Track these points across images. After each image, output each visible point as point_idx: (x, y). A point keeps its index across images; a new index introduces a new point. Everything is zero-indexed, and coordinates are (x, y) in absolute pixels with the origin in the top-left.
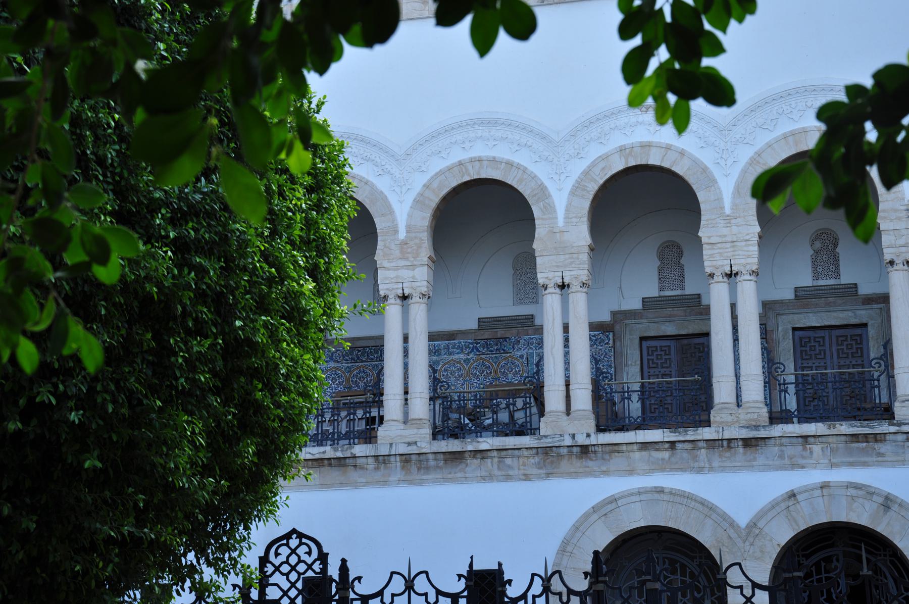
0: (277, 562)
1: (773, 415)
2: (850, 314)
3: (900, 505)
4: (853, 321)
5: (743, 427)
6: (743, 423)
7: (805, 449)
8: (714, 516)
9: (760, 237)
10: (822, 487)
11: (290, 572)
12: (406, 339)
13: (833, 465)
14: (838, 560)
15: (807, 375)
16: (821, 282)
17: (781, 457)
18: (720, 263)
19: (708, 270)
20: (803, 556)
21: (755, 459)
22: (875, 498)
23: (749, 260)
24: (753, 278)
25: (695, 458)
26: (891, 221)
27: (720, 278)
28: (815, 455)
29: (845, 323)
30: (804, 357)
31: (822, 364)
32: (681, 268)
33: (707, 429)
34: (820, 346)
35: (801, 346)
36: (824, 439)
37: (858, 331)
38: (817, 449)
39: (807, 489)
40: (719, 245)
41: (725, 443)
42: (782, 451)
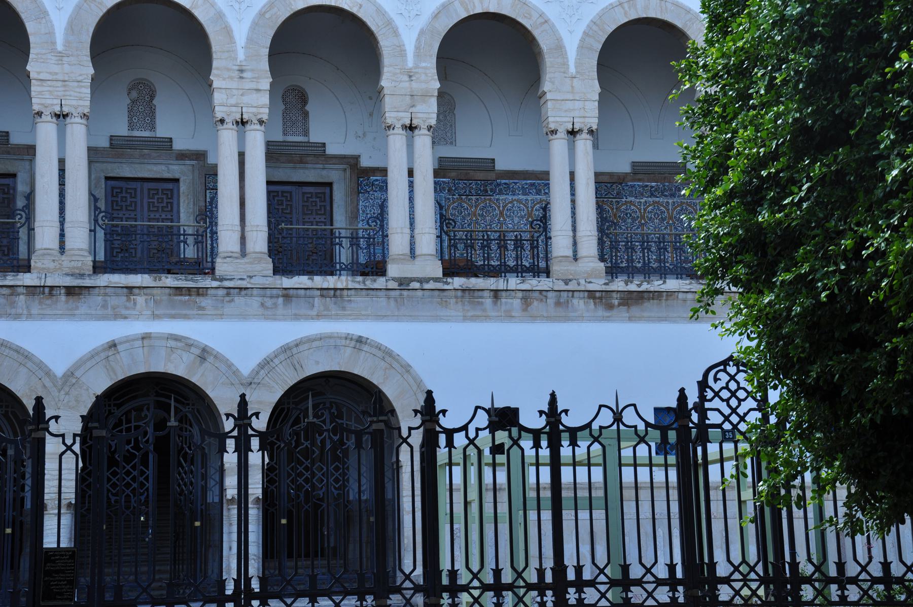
0: (717, 387)
1: (97, 264)
2: (163, 167)
3: (216, 357)
4: (167, 175)
5: (67, 275)
6: (67, 270)
7: (129, 300)
8: (29, 364)
9: (92, 79)
10: (143, 338)
11: (737, 398)
12: (411, 173)
13: (155, 317)
14: (148, 409)
15: (117, 226)
16: (136, 133)
17: (104, 306)
18: (49, 102)
19: (36, 108)
20: (115, 405)
21: (77, 308)
22: (193, 350)
23: (81, 103)
24: (84, 121)
25: (13, 305)
26: (224, 79)
27: (49, 118)
28: (138, 306)
29: (158, 176)
30: (115, 207)
31: (132, 216)
32: (306, 114)
33: (28, 275)
34: (131, 197)
35: (113, 196)
36: (148, 291)
37: (170, 186)
38: (140, 300)
39: (128, 340)
40: (49, 83)
41: (47, 290)
42: (106, 301)
